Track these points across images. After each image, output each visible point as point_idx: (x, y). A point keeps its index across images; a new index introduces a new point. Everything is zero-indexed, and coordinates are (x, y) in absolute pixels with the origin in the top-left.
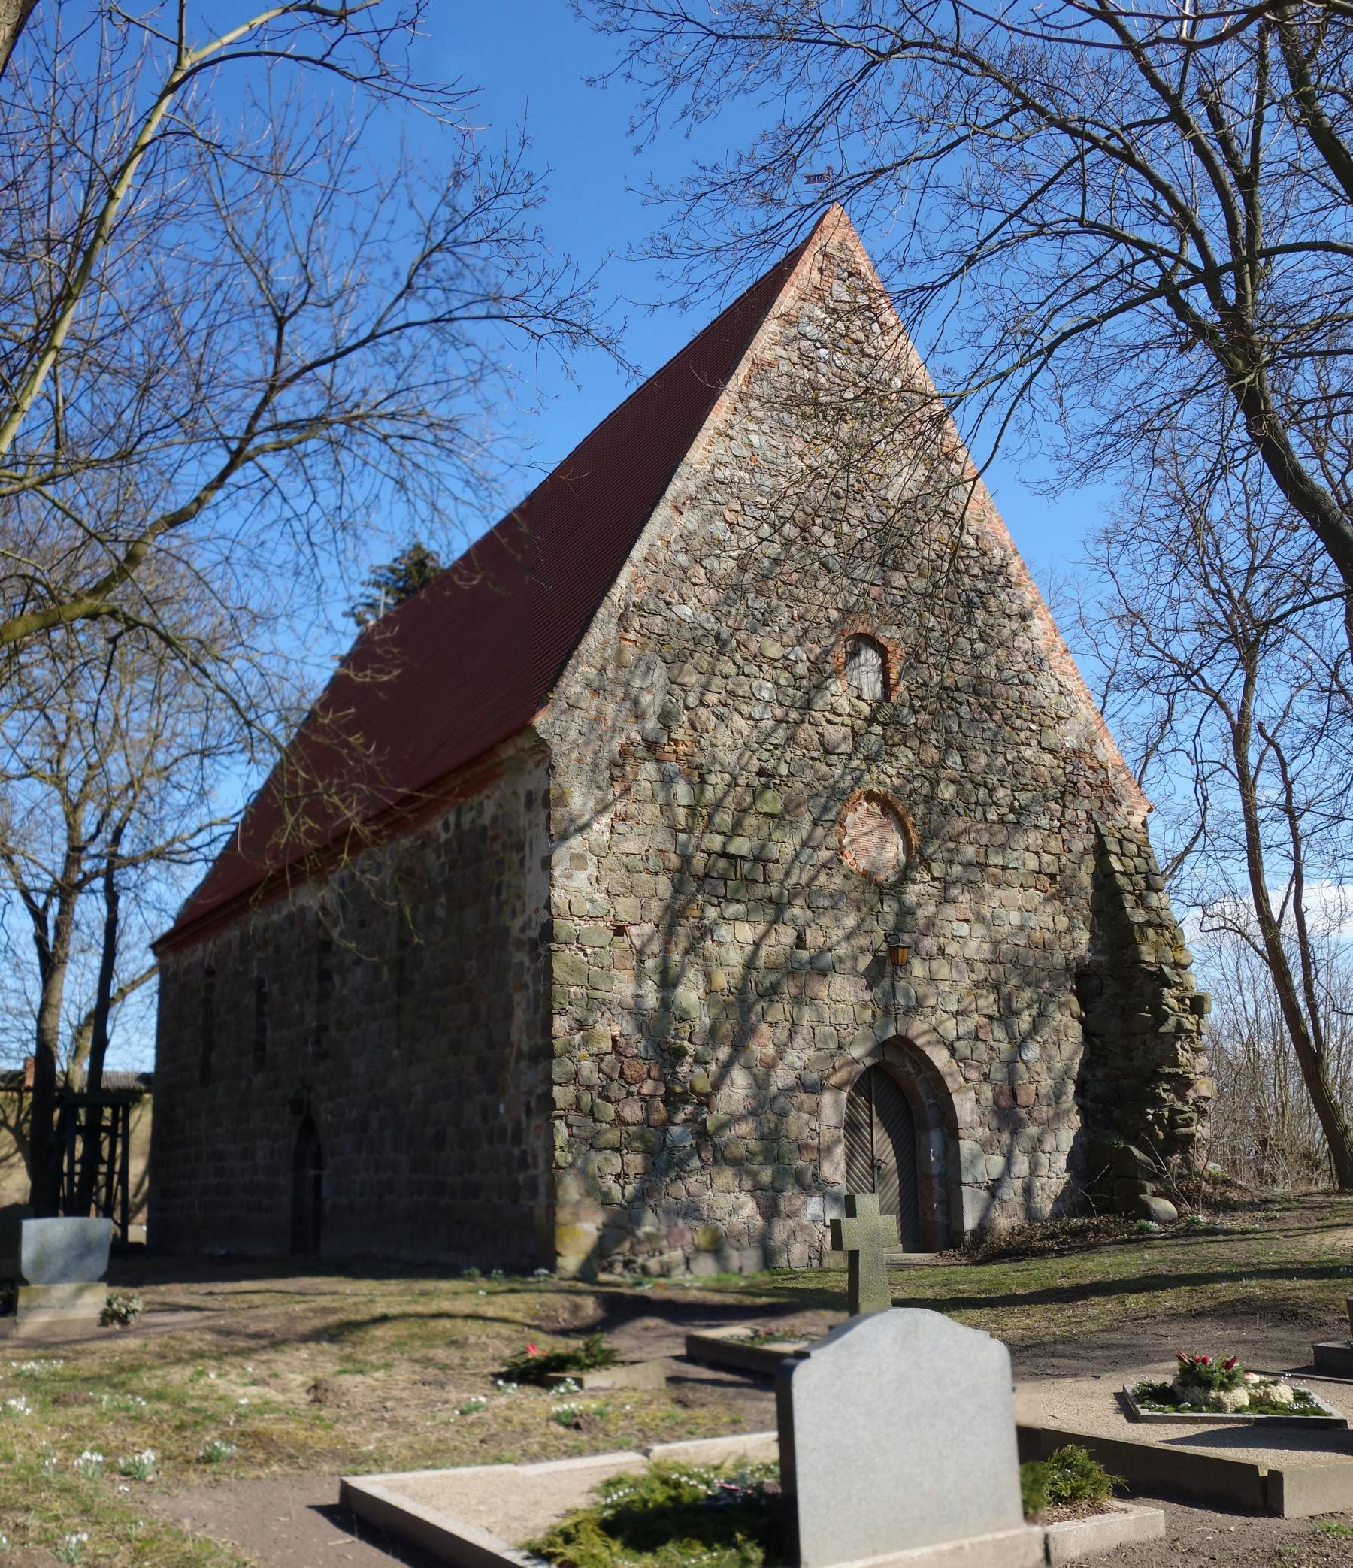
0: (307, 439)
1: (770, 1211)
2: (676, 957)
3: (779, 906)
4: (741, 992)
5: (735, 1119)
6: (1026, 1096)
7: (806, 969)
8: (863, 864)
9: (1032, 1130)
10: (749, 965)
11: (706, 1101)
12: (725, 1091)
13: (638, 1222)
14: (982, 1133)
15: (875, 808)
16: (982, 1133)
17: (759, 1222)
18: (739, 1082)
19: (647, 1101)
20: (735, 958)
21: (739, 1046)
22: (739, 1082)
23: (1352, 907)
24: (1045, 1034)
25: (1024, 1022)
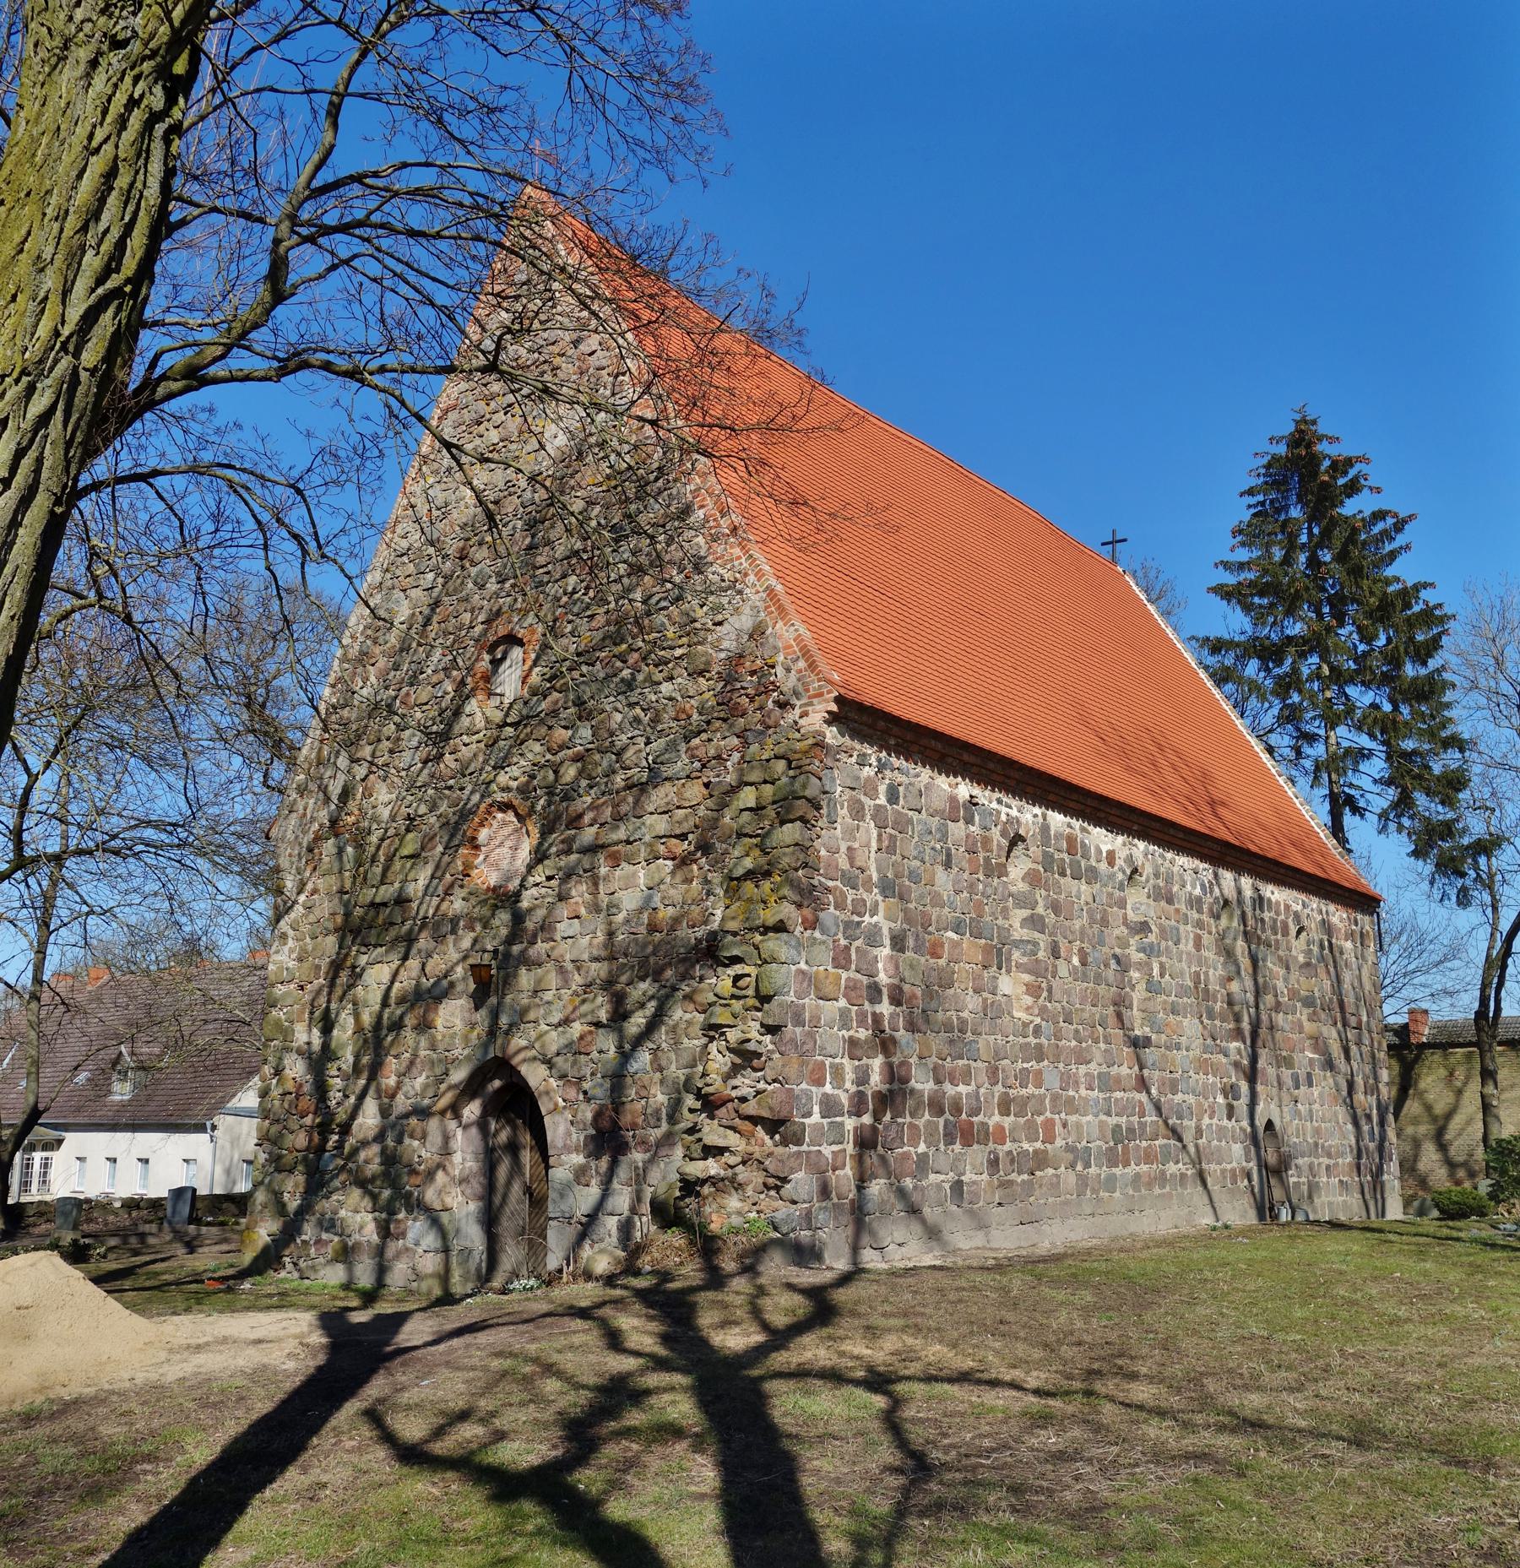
0: (1275, 988)
1: (385, 1231)
2: (333, 1006)
3: (410, 940)
4: (378, 1025)
5: (364, 1144)
6: (634, 1108)
7: (427, 997)
8: (493, 879)
9: (638, 1156)
10: (385, 1003)
11: (345, 1129)
12: (359, 1120)
13: (299, 1232)
14: (578, 1159)
15: (510, 816)
16: (578, 1159)
17: (375, 1238)
18: (371, 1107)
19: (310, 1130)
20: (375, 998)
21: (373, 1077)
22: (371, 1107)
23: (1513, 616)
24: (662, 1036)
25: (638, 1021)
